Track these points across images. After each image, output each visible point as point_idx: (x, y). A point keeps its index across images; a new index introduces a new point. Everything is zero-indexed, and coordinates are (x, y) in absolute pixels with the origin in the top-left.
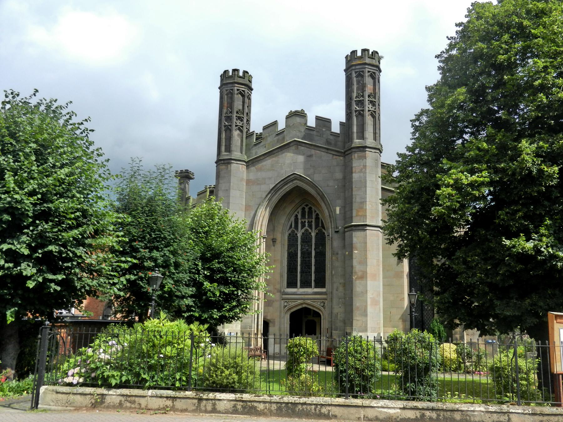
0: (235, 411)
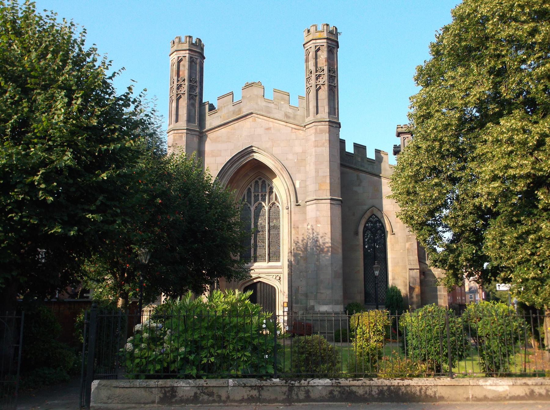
0: (331, 398)
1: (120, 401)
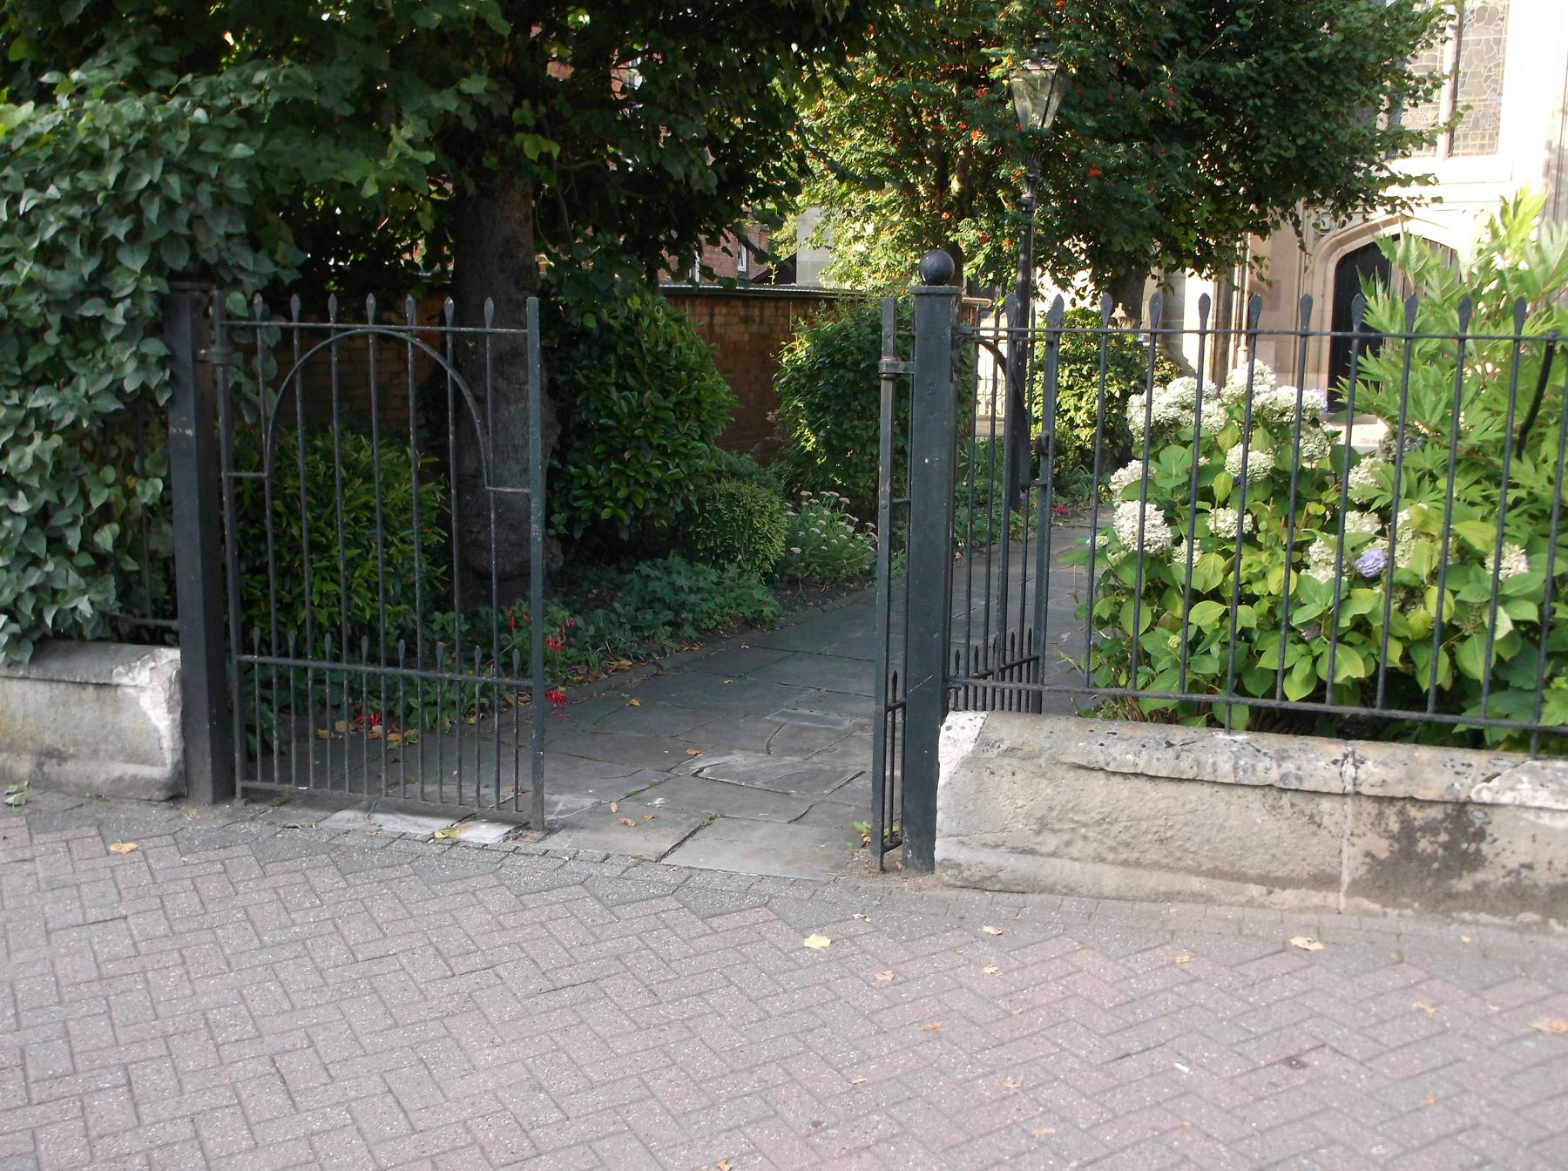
1: (1112, 849)
